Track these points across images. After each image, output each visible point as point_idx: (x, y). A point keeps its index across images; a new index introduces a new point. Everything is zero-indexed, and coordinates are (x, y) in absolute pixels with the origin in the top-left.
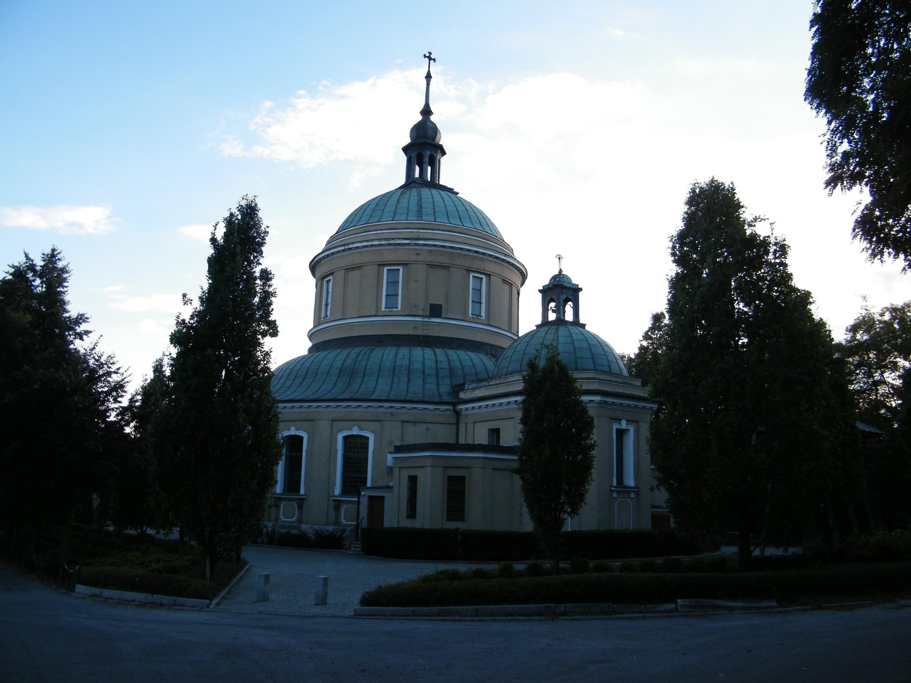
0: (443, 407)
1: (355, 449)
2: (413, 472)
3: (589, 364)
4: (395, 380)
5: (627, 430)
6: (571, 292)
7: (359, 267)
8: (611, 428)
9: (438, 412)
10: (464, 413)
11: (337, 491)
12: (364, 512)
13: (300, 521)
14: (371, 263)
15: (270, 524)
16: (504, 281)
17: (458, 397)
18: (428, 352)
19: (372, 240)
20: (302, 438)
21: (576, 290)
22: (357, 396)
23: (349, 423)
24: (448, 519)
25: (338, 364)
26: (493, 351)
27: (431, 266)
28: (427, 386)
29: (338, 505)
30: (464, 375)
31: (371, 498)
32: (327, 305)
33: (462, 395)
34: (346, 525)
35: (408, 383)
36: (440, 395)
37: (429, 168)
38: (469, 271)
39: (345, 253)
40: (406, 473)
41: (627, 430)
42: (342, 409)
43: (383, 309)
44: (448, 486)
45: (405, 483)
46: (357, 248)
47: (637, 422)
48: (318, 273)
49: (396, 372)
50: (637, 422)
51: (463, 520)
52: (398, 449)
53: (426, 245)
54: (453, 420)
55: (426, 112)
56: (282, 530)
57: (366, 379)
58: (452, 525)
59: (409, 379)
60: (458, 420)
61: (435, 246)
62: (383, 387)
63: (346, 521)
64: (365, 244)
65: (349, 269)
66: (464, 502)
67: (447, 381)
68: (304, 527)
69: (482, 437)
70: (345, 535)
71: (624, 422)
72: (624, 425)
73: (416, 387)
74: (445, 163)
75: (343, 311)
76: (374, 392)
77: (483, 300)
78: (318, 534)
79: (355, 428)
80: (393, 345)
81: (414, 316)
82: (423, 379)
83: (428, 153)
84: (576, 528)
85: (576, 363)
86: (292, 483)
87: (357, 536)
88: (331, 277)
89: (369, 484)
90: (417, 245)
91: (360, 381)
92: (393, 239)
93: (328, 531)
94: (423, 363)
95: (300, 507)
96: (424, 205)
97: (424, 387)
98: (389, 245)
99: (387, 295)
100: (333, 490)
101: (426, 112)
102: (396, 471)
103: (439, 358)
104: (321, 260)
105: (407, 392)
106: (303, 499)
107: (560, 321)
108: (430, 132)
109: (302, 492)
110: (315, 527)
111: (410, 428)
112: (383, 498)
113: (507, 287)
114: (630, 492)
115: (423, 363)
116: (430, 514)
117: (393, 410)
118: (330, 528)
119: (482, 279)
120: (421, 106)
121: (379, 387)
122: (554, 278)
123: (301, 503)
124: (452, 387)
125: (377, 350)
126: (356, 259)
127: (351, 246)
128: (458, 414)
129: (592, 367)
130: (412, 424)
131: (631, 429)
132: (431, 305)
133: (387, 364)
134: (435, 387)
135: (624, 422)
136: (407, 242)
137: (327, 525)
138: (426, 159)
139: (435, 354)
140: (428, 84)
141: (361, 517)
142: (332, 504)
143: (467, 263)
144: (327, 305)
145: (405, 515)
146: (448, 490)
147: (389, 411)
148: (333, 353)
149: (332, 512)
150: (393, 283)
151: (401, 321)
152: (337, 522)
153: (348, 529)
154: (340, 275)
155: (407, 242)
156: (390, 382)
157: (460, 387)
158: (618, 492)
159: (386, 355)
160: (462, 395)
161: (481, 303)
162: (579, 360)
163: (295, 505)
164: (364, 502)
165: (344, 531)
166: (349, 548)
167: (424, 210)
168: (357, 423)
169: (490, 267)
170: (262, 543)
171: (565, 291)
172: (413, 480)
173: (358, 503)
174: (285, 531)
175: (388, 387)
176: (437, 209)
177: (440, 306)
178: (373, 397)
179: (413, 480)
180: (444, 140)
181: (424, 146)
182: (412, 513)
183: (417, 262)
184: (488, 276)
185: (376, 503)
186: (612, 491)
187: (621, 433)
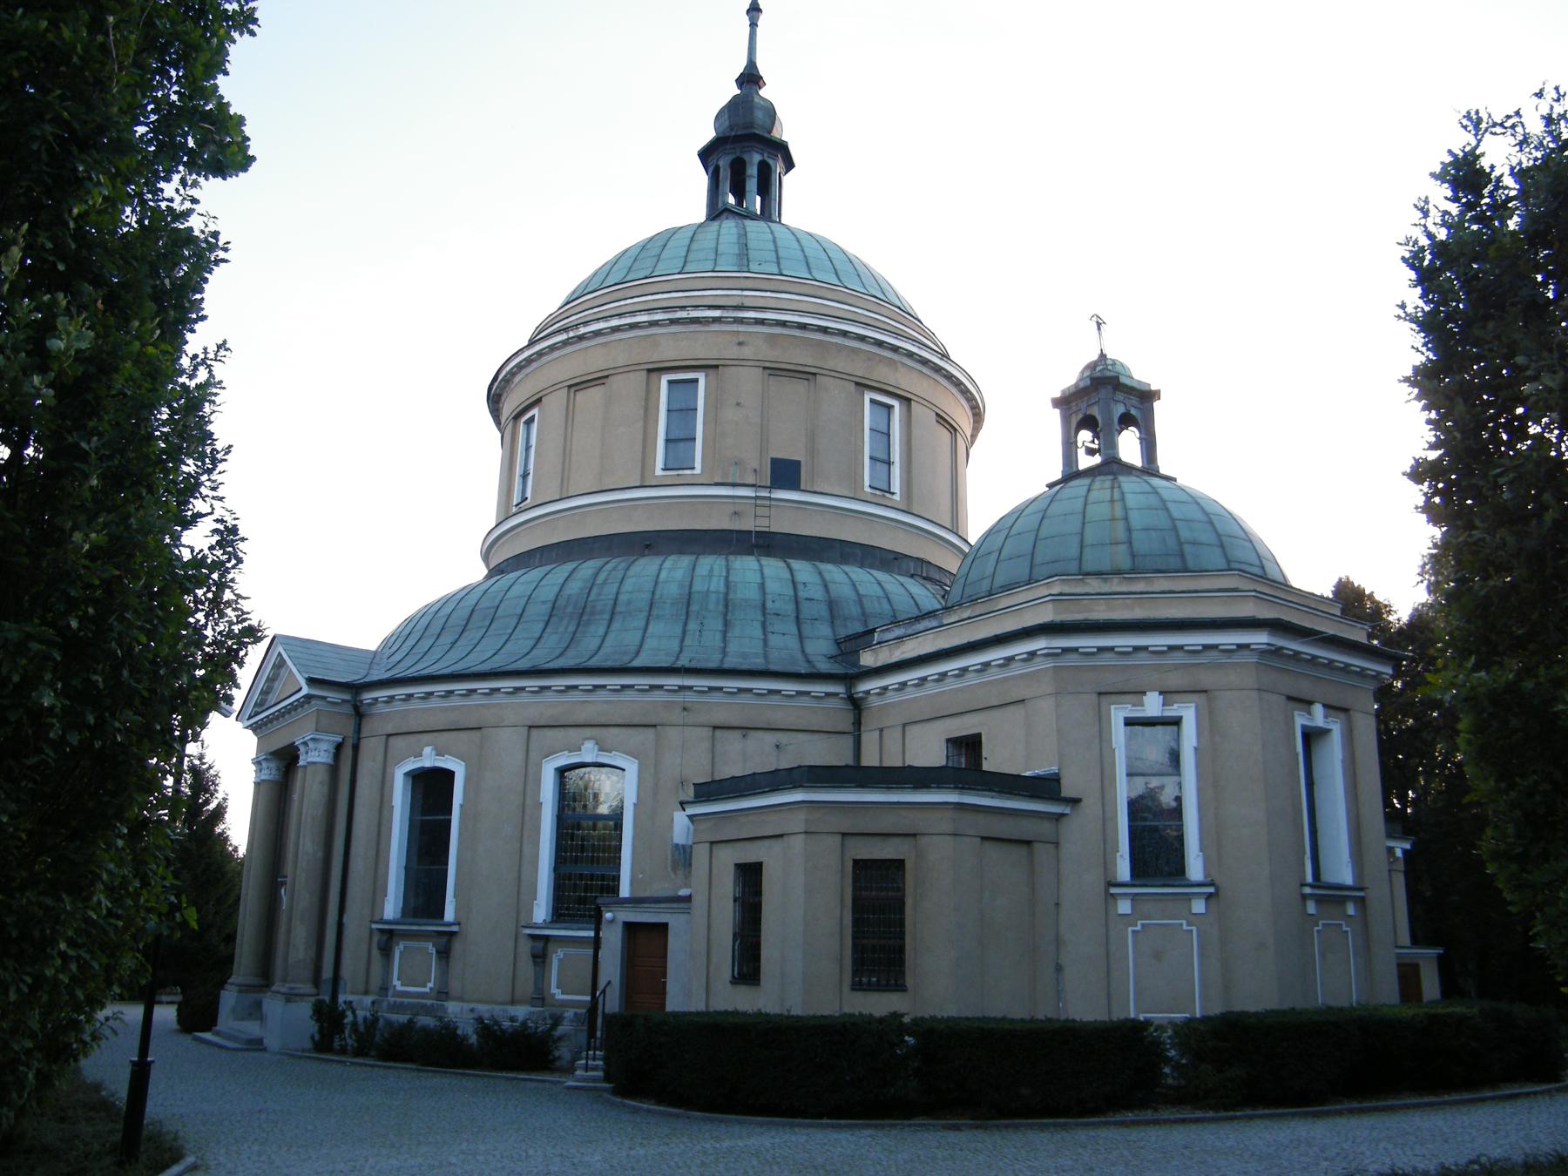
0: (819, 688)
1: (586, 847)
2: (750, 854)
3: (1215, 558)
4: (692, 626)
5: (1323, 733)
6: (1135, 401)
7: (600, 380)
8: (1290, 722)
9: (805, 702)
10: (874, 702)
11: (541, 911)
12: (611, 968)
13: (443, 993)
14: (629, 368)
15: (368, 1000)
16: (941, 419)
17: (856, 663)
18: (774, 567)
19: (633, 313)
20: (450, 775)
21: (1147, 397)
22: (593, 663)
23: (572, 732)
24: (857, 986)
25: (548, 592)
26: (922, 570)
27: (774, 371)
28: (774, 640)
29: (541, 948)
30: (865, 616)
31: (630, 927)
32: (525, 476)
33: (867, 659)
34: (565, 1004)
35: (725, 633)
36: (808, 661)
37: (758, 199)
38: (862, 386)
39: (569, 349)
40: (728, 858)
41: (1323, 733)
42: (551, 697)
43: (659, 472)
44: (855, 889)
45: (727, 886)
46: (597, 333)
47: (1345, 710)
48: (508, 409)
49: (694, 608)
50: (1345, 710)
51: (899, 987)
52: (708, 791)
53: (761, 322)
54: (845, 723)
55: (750, 78)
56: (394, 1017)
57: (616, 625)
58: (879, 1005)
59: (726, 624)
60: (858, 723)
61: (783, 324)
62: (660, 646)
63: (564, 989)
64: (615, 322)
65: (577, 386)
66: (901, 935)
67: (824, 630)
68: (452, 1008)
69: (928, 750)
70: (561, 1030)
71: (1318, 710)
72: (1318, 717)
73: (745, 646)
74: (792, 187)
75: (564, 480)
76: (638, 653)
77: (896, 456)
78: (487, 1030)
79: (589, 745)
80: (681, 552)
81: (734, 485)
82: (764, 625)
83: (757, 158)
84: (1216, 1009)
85: (1182, 556)
86: (426, 890)
87: (591, 1033)
88: (535, 411)
89: (625, 891)
90: (740, 321)
91: (601, 631)
92: (683, 308)
93: (512, 1019)
94: (762, 586)
95: (444, 954)
96: (751, 244)
97: (765, 641)
98: (673, 322)
99: (668, 441)
100: (531, 911)
101: (750, 78)
102: (700, 855)
103: (800, 577)
104: (512, 373)
105: (724, 652)
106: (452, 934)
107: (1112, 466)
108: (759, 115)
109: (449, 914)
110: (484, 1009)
111: (732, 744)
112: (663, 928)
113: (945, 435)
114: (1342, 901)
115: (762, 586)
116: (804, 972)
117: (689, 697)
118: (521, 1012)
119: (889, 408)
120: (739, 67)
121: (650, 643)
122: (1092, 366)
123: (446, 943)
124: (838, 643)
125: (643, 561)
126: (590, 360)
127: (582, 330)
128: (856, 705)
129: (1222, 564)
130: (738, 734)
131: (1336, 729)
132: (775, 462)
133: (671, 590)
134: (793, 643)
135: (1318, 710)
136: (717, 313)
137: (513, 1002)
138: (752, 171)
139: (789, 566)
140: (753, 25)
141: (602, 984)
142: (525, 948)
143: (859, 369)
144: (525, 476)
145: (727, 975)
146: (855, 900)
147: (678, 698)
148: (535, 574)
149: (527, 968)
150: (682, 412)
151: (703, 496)
152: (540, 998)
153: (569, 1013)
154: (556, 402)
155: (717, 313)
156: (678, 630)
157: (864, 638)
158: (1319, 900)
159: (674, 569)
160: (867, 659)
161: (889, 463)
162: (1188, 549)
163: (432, 949)
164: (612, 938)
165: (557, 1021)
166: (570, 1070)
167: (752, 254)
168: (588, 732)
169: (907, 380)
170: (343, 1051)
171: (1120, 396)
172: (750, 875)
173: (596, 943)
174: (403, 1018)
175: (675, 644)
176: (782, 253)
177: (798, 463)
178: (637, 663)
179: (750, 875)
180: (789, 130)
181: (746, 152)
182: (748, 967)
183: (740, 362)
184: (906, 401)
185: (646, 943)
186: (1304, 897)
187: (1312, 737)
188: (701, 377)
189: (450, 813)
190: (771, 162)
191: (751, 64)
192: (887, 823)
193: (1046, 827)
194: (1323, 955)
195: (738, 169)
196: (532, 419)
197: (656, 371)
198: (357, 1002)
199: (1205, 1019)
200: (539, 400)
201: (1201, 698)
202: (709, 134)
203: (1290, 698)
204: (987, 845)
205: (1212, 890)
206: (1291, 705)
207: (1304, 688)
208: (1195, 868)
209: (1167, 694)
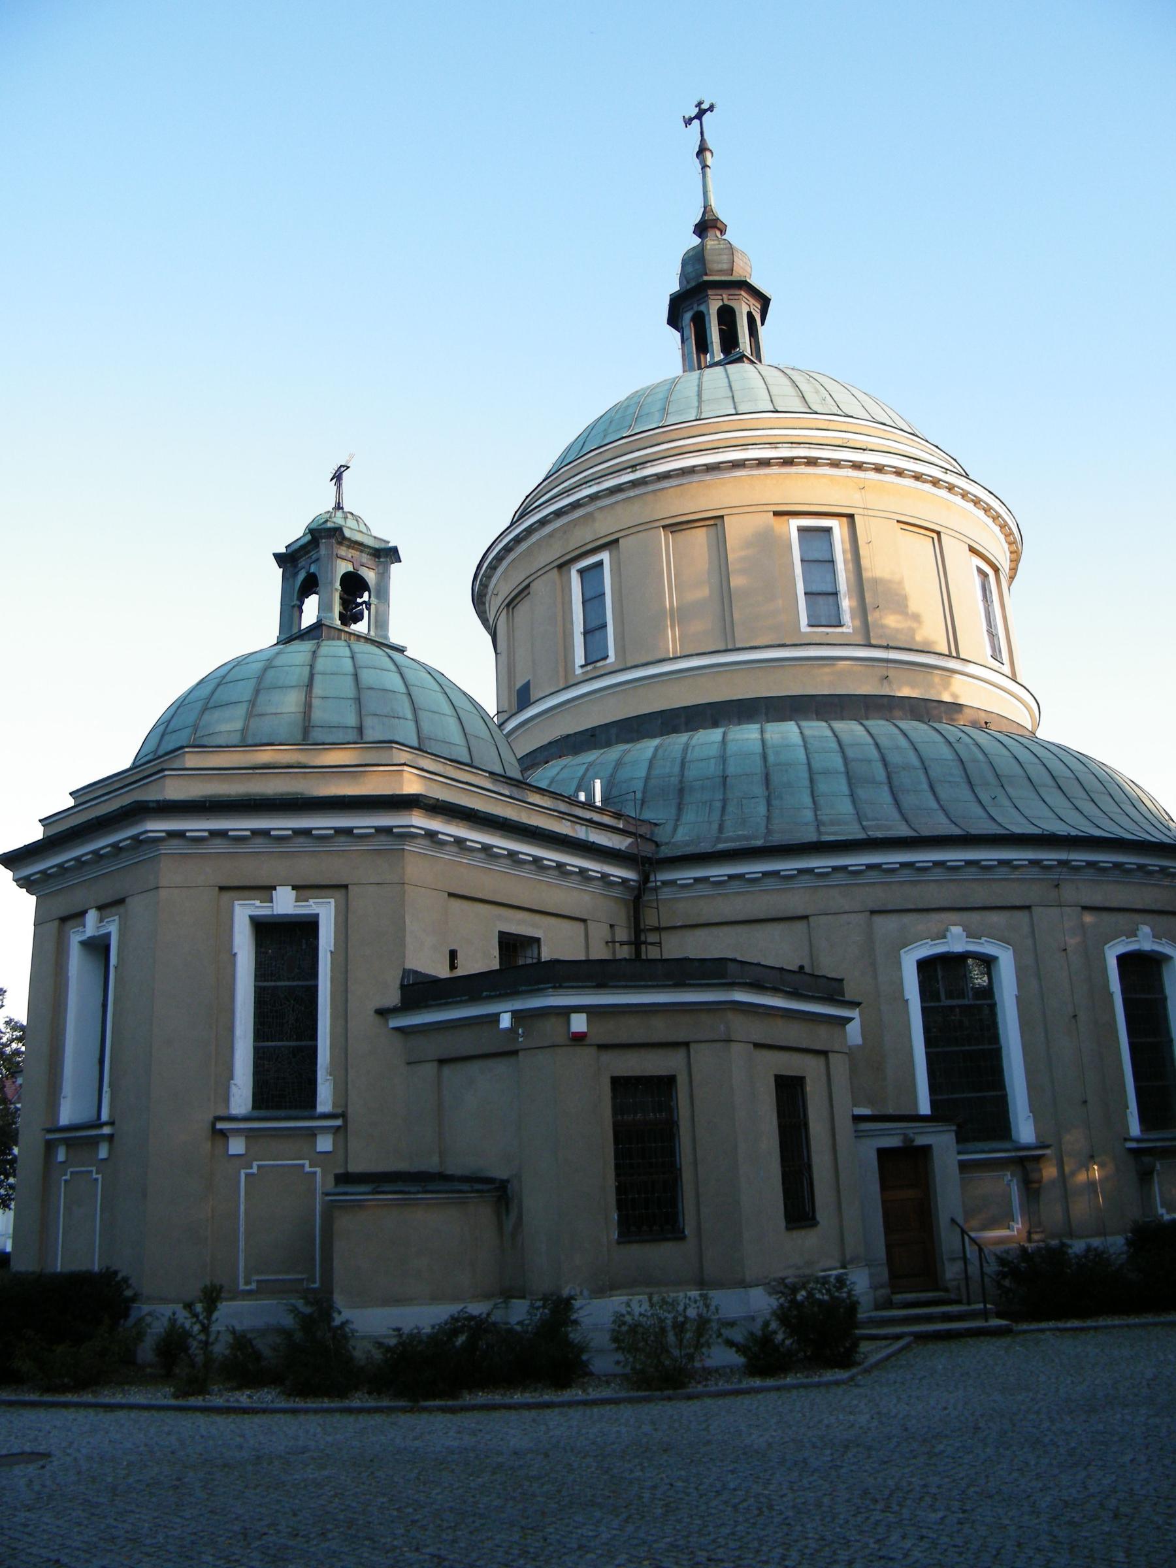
18: (817, 729)
55: (707, 225)
79: (956, 930)
114: (94, 1142)
172: (789, 1090)
189: (314, 1036)
190: (732, 304)
191: (707, 208)
192: (660, 1029)
194: (68, 1208)
195: (700, 322)
197: (563, 567)
198: (483, 1213)
199: (61, 1273)
201: (340, 894)
205: (339, 1122)
208: (325, 1098)
209: (302, 889)
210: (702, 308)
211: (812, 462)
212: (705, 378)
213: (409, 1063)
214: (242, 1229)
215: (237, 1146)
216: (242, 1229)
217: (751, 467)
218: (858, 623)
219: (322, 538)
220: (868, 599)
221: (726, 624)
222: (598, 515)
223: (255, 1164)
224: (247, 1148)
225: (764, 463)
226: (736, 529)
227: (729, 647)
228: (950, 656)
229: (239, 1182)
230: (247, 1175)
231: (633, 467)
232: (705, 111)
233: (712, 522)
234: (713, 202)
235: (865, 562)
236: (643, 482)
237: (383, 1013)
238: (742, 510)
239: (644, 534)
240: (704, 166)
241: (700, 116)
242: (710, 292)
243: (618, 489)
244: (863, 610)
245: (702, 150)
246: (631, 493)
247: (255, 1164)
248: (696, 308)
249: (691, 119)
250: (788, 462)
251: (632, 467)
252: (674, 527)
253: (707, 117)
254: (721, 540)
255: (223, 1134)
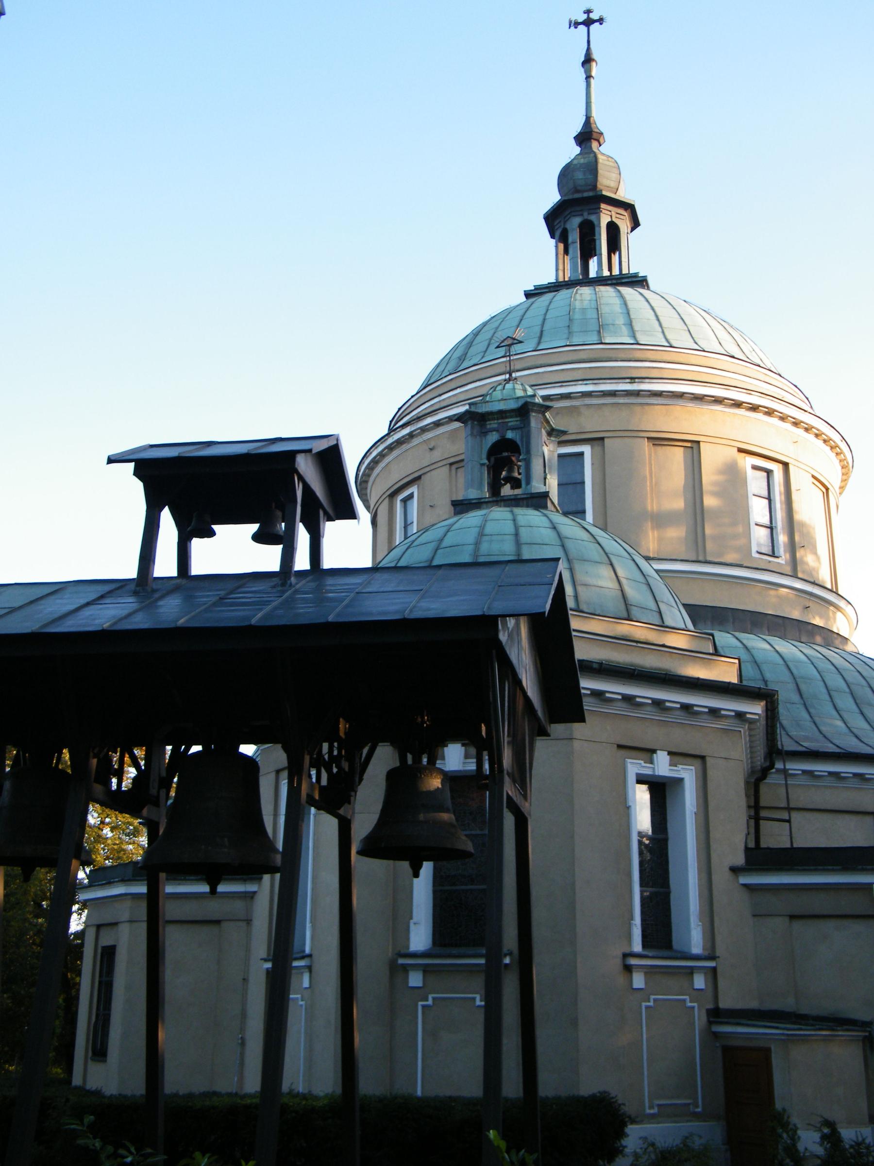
55: (587, 136)
88: (414, 489)
101: (587, 136)
119: (769, 473)
120: (577, 127)
131: (688, 774)
188: (586, 449)
193: (239, 906)
195: (588, 232)
196: (411, 496)
200: (419, 478)
202: (553, 197)
203: (620, 747)
204: (797, 925)
206: (623, 752)
207: (646, 735)
210: (593, 218)
211: (770, 412)
212: (554, 278)
213: (754, 916)
214: (645, 1057)
215: (415, 979)
216: (645, 1057)
217: (727, 406)
218: (788, 556)
219: (533, 411)
220: (797, 538)
221: (697, 537)
222: (583, 410)
223: (652, 997)
224: (646, 983)
225: (738, 404)
226: (712, 458)
227: (701, 558)
228: (831, 591)
229: (641, 1014)
230: (423, 1006)
231: (633, 380)
232: (594, 22)
233: (689, 445)
234: (594, 114)
235: (796, 506)
236: (637, 393)
237: (735, 870)
238: (717, 440)
239: (619, 440)
240: (589, 77)
241: (588, 23)
242: (603, 206)
243: (613, 394)
244: (792, 547)
245: (588, 60)
246: (621, 400)
247: (430, 997)
248: (586, 216)
249: (577, 24)
250: (754, 408)
251: (631, 378)
252: (658, 441)
253: (595, 27)
254: (696, 464)
255: (405, 969)
